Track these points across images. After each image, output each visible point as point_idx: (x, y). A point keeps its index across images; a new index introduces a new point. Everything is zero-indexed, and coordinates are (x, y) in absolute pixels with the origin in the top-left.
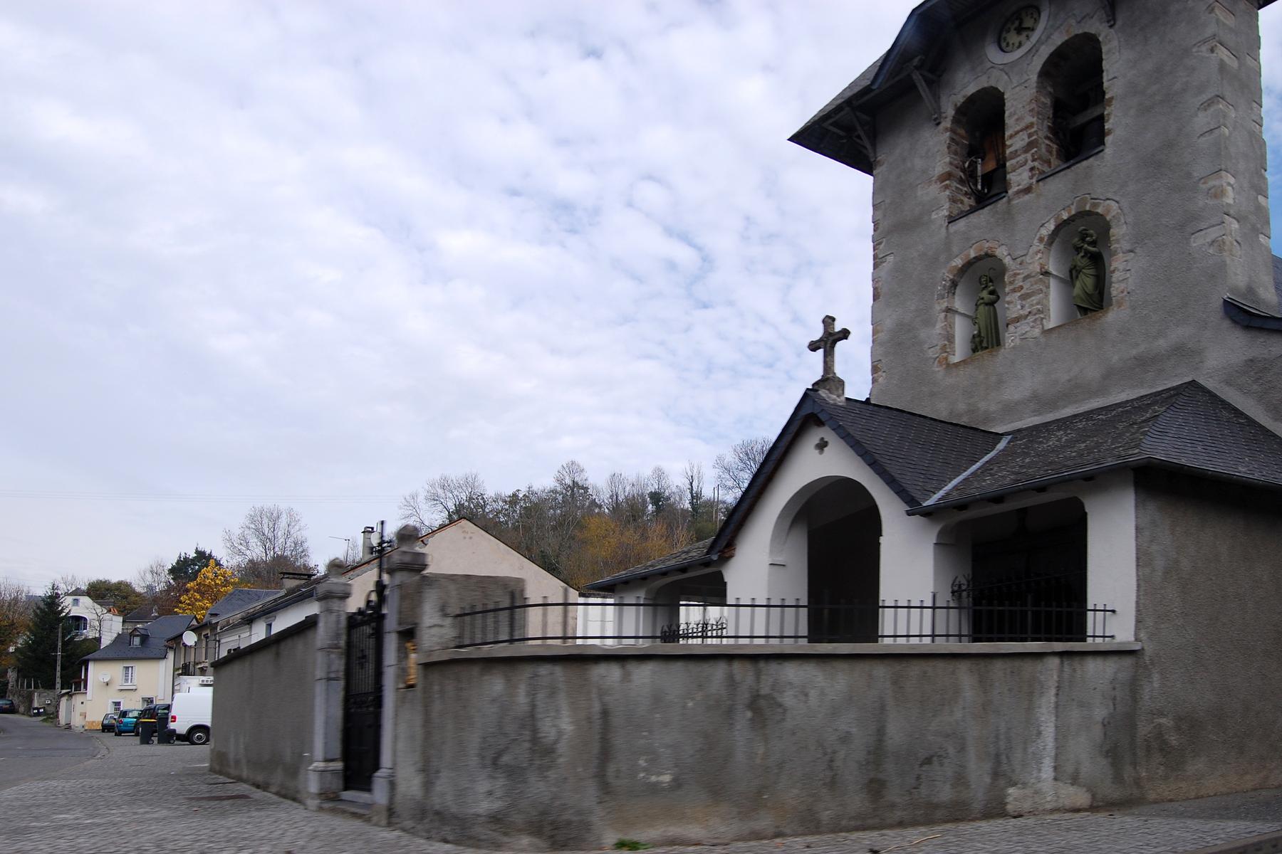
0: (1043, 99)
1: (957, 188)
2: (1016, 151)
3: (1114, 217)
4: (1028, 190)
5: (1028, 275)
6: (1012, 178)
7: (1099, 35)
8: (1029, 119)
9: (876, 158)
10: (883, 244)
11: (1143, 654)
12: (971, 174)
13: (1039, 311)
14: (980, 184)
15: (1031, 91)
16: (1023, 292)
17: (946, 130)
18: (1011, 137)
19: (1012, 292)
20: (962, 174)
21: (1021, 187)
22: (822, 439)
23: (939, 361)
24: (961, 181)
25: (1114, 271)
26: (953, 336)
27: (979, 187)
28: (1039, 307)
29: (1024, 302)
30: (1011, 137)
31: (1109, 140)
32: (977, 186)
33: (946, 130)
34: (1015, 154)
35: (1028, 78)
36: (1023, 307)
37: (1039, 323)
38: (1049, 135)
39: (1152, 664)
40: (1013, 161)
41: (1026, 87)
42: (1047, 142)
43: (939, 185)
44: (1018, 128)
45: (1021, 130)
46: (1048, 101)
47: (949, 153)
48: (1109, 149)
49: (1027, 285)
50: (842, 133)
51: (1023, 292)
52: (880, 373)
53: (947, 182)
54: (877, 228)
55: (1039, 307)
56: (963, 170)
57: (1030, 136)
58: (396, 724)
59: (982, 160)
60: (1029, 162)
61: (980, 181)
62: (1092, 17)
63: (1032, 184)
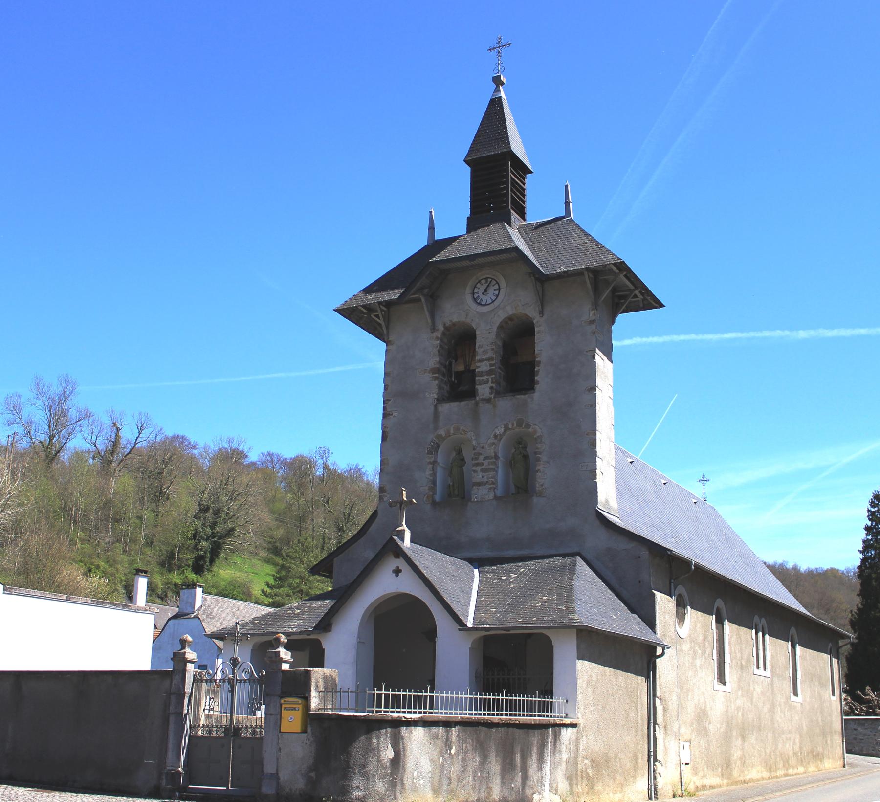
0: (498, 343)
1: (441, 379)
2: (482, 372)
3: (538, 437)
4: (488, 401)
5: (487, 457)
6: (479, 389)
7: (534, 319)
8: (490, 354)
9: (388, 338)
10: (391, 401)
11: (580, 726)
12: (449, 368)
13: (493, 483)
14: (453, 377)
15: (493, 336)
16: (483, 467)
17: (437, 338)
18: (480, 361)
19: (715, 787)
20: (444, 370)
21: (484, 397)
22: (398, 567)
23: (427, 497)
24: (444, 375)
25: (537, 472)
26: (436, 482)
27: (453, 379)
28: (493, 480)
29: (484, 474)
30: (480, 361)
31: (537, 387)
32: (451, 379)
33: (437, 338)
34: (481, 374)
35: (491, 327)
36: (483, 477)
37: (492, 490)
38: (501, 366)
39: (583, 731)
40: (481, 378)
41: (490, 332)
42: (499, 370)
43: (431, 375)
44: (484, 357)
45: (486, 360)
46: (500, 343)
47: (439, 355)
48: (536, 395)
49: (486, 462)
50: (365, 311)
51: (483, 467)
52: (385, 494)
53: (437, 375)
54: (387, 389)
55: (493, 480)
56: (445, 367)
57: (491, 365)
58: (551, 758)
59: (455, 362)
60: (490, 383)
61: (453, 375)
62: (530, 306)
63: (491, 398)
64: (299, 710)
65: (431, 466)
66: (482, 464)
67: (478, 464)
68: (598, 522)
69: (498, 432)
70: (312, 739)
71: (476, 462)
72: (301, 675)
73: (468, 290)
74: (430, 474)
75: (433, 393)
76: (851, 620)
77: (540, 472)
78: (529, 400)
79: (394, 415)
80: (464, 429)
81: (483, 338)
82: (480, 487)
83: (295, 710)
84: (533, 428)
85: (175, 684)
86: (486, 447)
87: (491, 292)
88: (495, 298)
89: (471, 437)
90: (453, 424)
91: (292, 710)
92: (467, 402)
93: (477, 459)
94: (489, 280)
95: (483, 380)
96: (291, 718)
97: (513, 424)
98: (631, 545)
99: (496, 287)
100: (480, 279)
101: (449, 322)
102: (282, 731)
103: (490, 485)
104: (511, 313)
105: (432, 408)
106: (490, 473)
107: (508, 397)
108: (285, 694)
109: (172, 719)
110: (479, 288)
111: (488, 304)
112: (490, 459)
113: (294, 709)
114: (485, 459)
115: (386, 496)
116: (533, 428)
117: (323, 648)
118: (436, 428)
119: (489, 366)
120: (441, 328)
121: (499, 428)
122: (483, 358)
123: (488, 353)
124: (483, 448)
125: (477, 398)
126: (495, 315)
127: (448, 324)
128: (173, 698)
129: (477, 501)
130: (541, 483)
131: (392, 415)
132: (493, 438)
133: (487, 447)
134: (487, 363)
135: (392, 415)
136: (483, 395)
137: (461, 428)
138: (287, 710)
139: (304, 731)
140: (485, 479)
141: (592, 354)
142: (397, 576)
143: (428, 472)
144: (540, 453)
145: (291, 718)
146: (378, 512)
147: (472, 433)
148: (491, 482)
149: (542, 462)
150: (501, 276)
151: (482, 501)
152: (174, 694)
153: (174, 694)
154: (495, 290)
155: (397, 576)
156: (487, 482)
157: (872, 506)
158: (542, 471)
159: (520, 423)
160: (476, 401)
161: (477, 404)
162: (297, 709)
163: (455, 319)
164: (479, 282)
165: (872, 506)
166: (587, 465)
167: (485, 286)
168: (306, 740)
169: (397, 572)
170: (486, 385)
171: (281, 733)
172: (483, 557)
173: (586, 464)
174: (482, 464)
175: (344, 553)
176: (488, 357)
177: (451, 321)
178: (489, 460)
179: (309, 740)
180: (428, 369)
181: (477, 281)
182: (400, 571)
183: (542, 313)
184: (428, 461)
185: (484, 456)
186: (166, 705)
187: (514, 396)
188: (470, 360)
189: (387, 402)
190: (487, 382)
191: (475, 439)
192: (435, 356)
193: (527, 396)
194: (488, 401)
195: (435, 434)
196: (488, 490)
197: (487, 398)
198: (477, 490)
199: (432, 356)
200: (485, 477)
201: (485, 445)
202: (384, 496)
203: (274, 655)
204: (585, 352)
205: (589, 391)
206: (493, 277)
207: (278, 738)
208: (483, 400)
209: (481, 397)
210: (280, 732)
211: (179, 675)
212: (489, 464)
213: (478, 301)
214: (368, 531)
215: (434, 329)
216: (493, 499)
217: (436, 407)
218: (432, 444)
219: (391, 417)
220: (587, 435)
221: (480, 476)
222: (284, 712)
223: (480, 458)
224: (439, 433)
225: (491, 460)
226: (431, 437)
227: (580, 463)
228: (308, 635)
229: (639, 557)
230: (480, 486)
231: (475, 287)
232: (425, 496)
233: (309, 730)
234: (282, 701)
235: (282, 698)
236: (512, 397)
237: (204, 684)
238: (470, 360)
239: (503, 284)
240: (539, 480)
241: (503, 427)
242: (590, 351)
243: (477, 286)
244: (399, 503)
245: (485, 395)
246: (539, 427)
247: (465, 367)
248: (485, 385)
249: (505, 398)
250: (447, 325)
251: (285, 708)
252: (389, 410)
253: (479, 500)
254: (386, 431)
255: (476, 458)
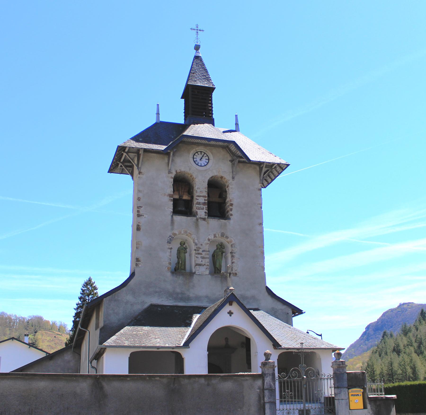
2: (200, 203)
16: (202, 256)
23: (168, 268)
29: (203, 260)
41: (204, 182)
44: (201, 195)
48: (231, 221)
49: (204, 253)
51: (202, 256)
64: (361, 396)
65: (170, 250)
66: (201, 254)
67: (199, 254)
68: (267, 294)
69: (210, 238)
70: (371, 412)
71: (198, 252)
72: (359, 375)
73: (191, 155)
74: (169, 255)
75: (170, 208)
76: (66, 343)
77: (235, 263)
78: (228, 223)
79: (144, 216)
80: (190, 232)
81: (200, 184)
82: (200, 267)
83: (359, 396)
84: (230, 239)
85: (267, 383)
86: (204, 244)
87: (204, 159)
88: (207, 164)
89: (194, 237)
90: (183, 229)
91: (356, 396)
92: (191, 217)
93: (198, 251)
94: (203, 153)
95: (200, 207)
96: (357, 401)
97: (218, 235)
98: (284, 307)
99: (207, 158)
100: (198, 151)
101: (179, 170)
102: (351, 409)
103: (207, 266)
104: (216, 174)
105: (170, 217)
106: (206, 260)
107: (216, 219)
108: (350, 387)
109: (267, 406)
110: (197, 156)
111: (202, 166)
112: (206, 252)
113: (358, 395)
114: (203, 251)
115: (141, 264)
116: (230, 239)
117: (321, 358)
118: (172, 229)
119: (204, 200)
120: (174, 173)
121: (211, 235)
122: (200, 195)
123: (203, 193)
124: (202, 245)
125: (197, 217)
126: (207, 173)
127: (178, 171)
128: (266, 392)
129: (199, 275)
130: (236, 269)
131: (143, 216)
132: (208, 241)
133: (204, 244)
134: (203, 198)
135: (143, 216)
136: (201, 215)
137: (188, 232)
138: (353, 396)
139: (365, 407)
140: (203, 263)
141: (261, 206)
142: (230, 316)
143: (168, 254)
144: (235, 253)
145: (357, 401)
146: (135, 273)
147: (195, 235)
148: (207, 265)
149: (235, 258)
150: (210, 153)
151: (202, 275)
152: (267, 389)
153: (267, 389)
154: (206, 159)
155: (230, 316)
156: (205, 264)
157: (83, 287)
158: (235, 262)
159: (223, 235)
160: (197, 218)
161: (197, 220)
162: (360, 395)
163: (183, 170)
164: (197, 152)
165: (83, 287)
166: (260, 263)
167: (201, 156)
168: (368, 413)
169: (230, 313)
170: (203, 210)
171: (351, 410)
172: (204, 306)
173: (259, 262)
174: (201, 254)
175: (111, 296)
176: (203, 195)
177: (180, 170)
178: (206, 253)
179: (369, 413)
180: (167, 194)
181: (196, 152)
182: (232, 313)
183: (233, 178)
184: (168, 247)
185: (202, 250)
186: (261, 397)
187: (219, 219)
188: (182, 194)
189: (140, 208)
190: (203, 209)
191: (197, 239)
192: (171, 187)
193: (226, 221)
194: (204, 219)
195: (172, 233)
196: (205, 269)
197: (203, 218)
198: (198, 268)
199: (168, 187)
200: (204, 262)
201: (203, 243)
202: (139, 263)
203: (341, 363)
204: (257, 204)
205: (259, 225)
206: (205, 152)
207: (350, 413)
208: (201, 218)
209: (200, 216)
210: (350, 409)
211: (269, 377)
212: (205, 255)
213: (197, 163)
214: (128, 284)
215: (170, 172)
216: (209, 274)
217: (172, 216)
218: (170, 238)
219: (143, 217)
220: (259, 247)
221: (201, 261)
222: (351, 398)
223: (200, 251)
224: (175, 232)
225: (207, 253)
226: (169, 233)
227: (256, 262)
228: (158, 349)
229: (288, 314)
230: (200, 266)
231: (194, 155)
232: (166, 267)
233: (369, 406)
234: (350, 391)
235: (349, 389)
236: (218, 220)
237: (326, 381)
238: (182, 194)
239: (211, 157)
240: (234, 268)
241: (213, 235)
242: (259, 204)
243: (195, 154)
244: (228, 273)
245: (202, 215)
246: (233, 239)
247: (180, 197)
248: (201, 210)
249: (214, 219)
250: (178, 172)
251: (352, 395)
252: (142, 213)
253: (200, 274)
254: (140, 225)
255: (197, 250)
